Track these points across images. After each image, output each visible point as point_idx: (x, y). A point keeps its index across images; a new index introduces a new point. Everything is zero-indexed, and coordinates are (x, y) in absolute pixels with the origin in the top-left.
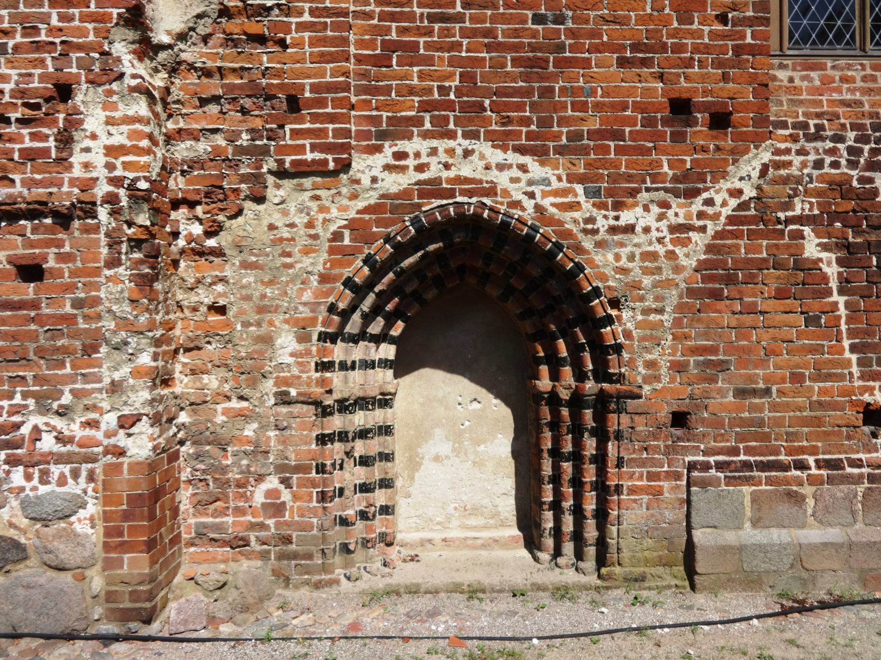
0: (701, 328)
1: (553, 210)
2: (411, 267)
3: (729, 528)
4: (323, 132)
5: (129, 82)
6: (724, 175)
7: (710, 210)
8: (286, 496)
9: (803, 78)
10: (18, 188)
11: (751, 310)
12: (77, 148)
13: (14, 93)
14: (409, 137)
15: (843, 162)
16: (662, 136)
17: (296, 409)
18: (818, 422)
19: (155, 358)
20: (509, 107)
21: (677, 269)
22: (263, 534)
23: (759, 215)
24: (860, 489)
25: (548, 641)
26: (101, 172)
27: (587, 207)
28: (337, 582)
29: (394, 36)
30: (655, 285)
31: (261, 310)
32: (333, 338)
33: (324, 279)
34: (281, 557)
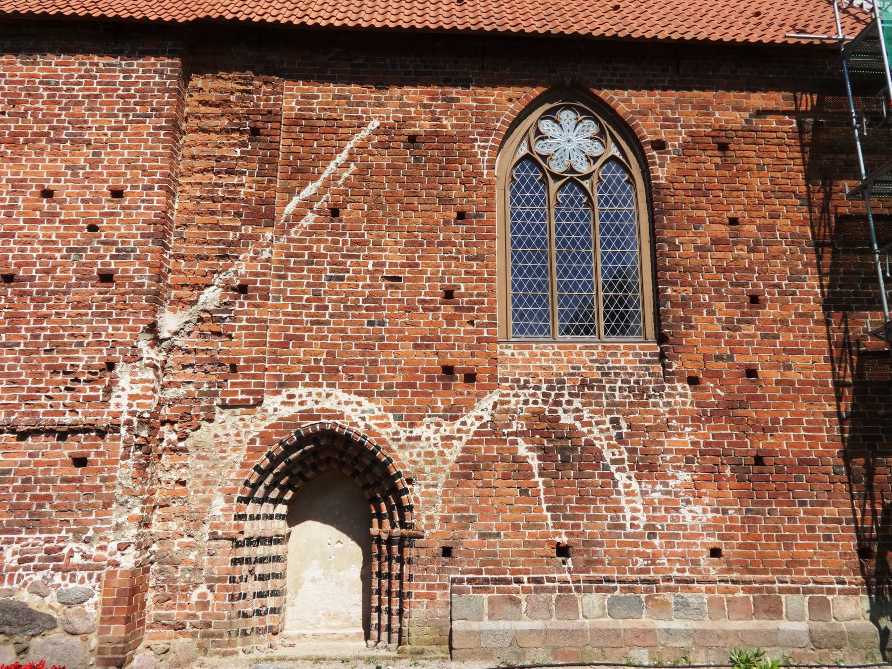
0: (459, 496)
1: (375, 427)
2: (296, 458)
3: (474, 620)
4: (248, 384)
5: (145, 361)
6: (473, 408)
7: (464, 428)
8: (210, 597)
9: (520, 354)
10: (80, 417)
11: (488, 486)
12: (113, 395)
13: (84, 367)
14: (297, 386)
15: (540, 401)
16: (438, 386)
17: (221, 543)
18: (529, 554)
19: (142, 510)
20: (352, 370)
21: (445, 462)
22: (194, 621)
23: (491, 432)
24: (554, 596)
26: (125, 409)
27: (395, 426)
28: (236, 653)
29: (291, 332)
30: (432, 471)
31: (206, 483)
32: (246, 501)
33: (243, 465)
34: (204, 636)
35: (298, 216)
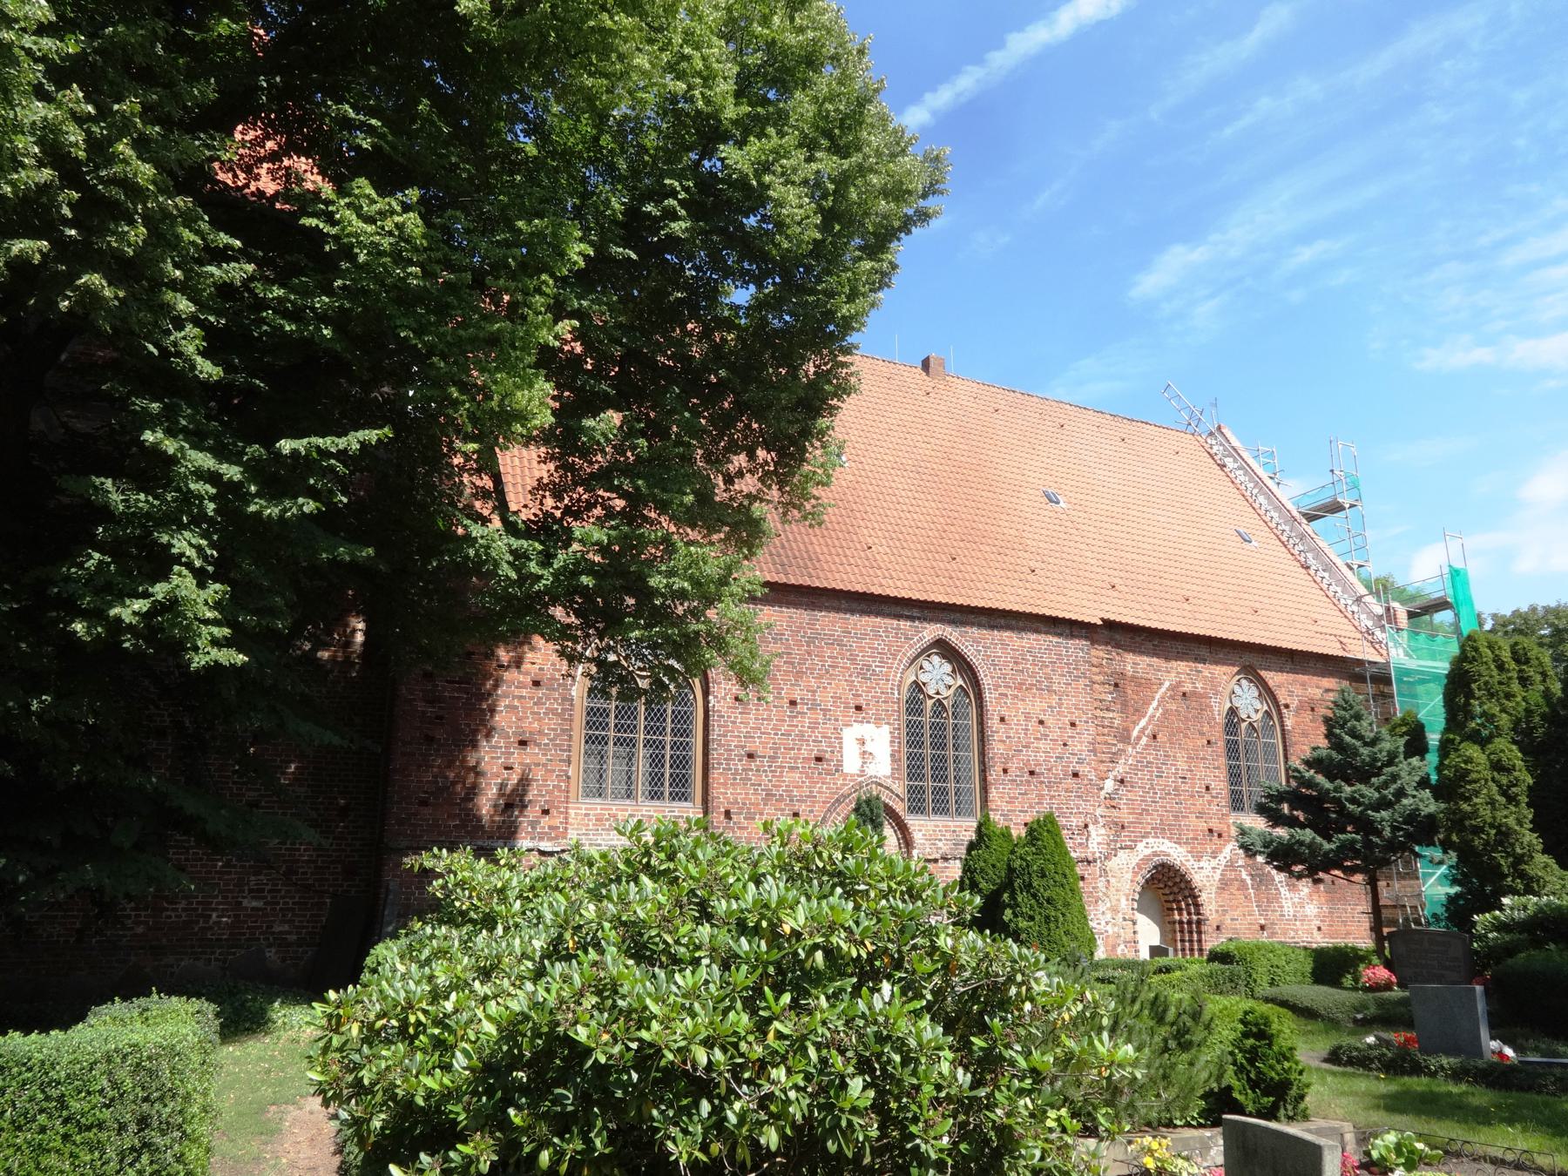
25: (994, 774)
35: (1139, 738)
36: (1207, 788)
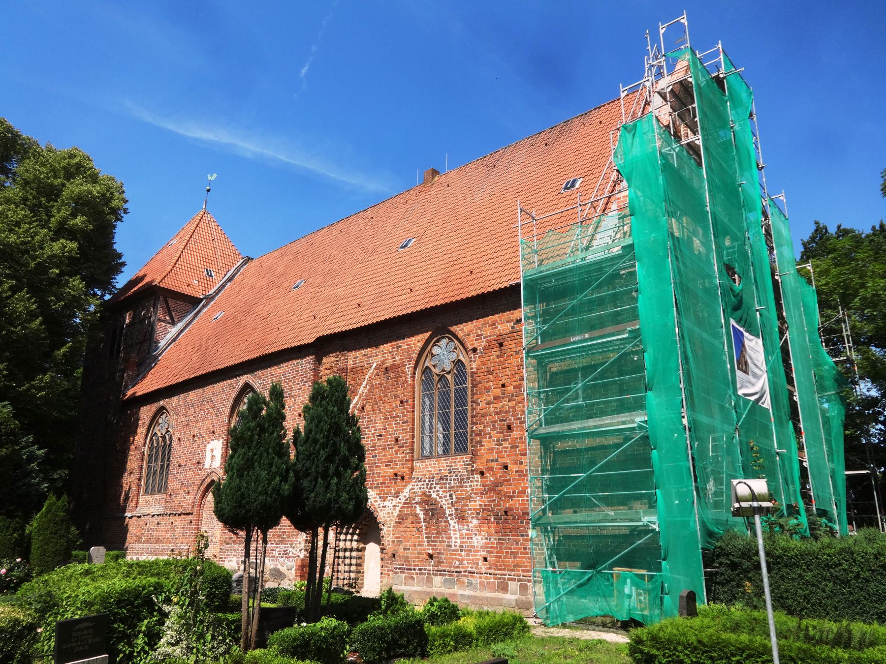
23: (408, 503)
36: (397, 440)
